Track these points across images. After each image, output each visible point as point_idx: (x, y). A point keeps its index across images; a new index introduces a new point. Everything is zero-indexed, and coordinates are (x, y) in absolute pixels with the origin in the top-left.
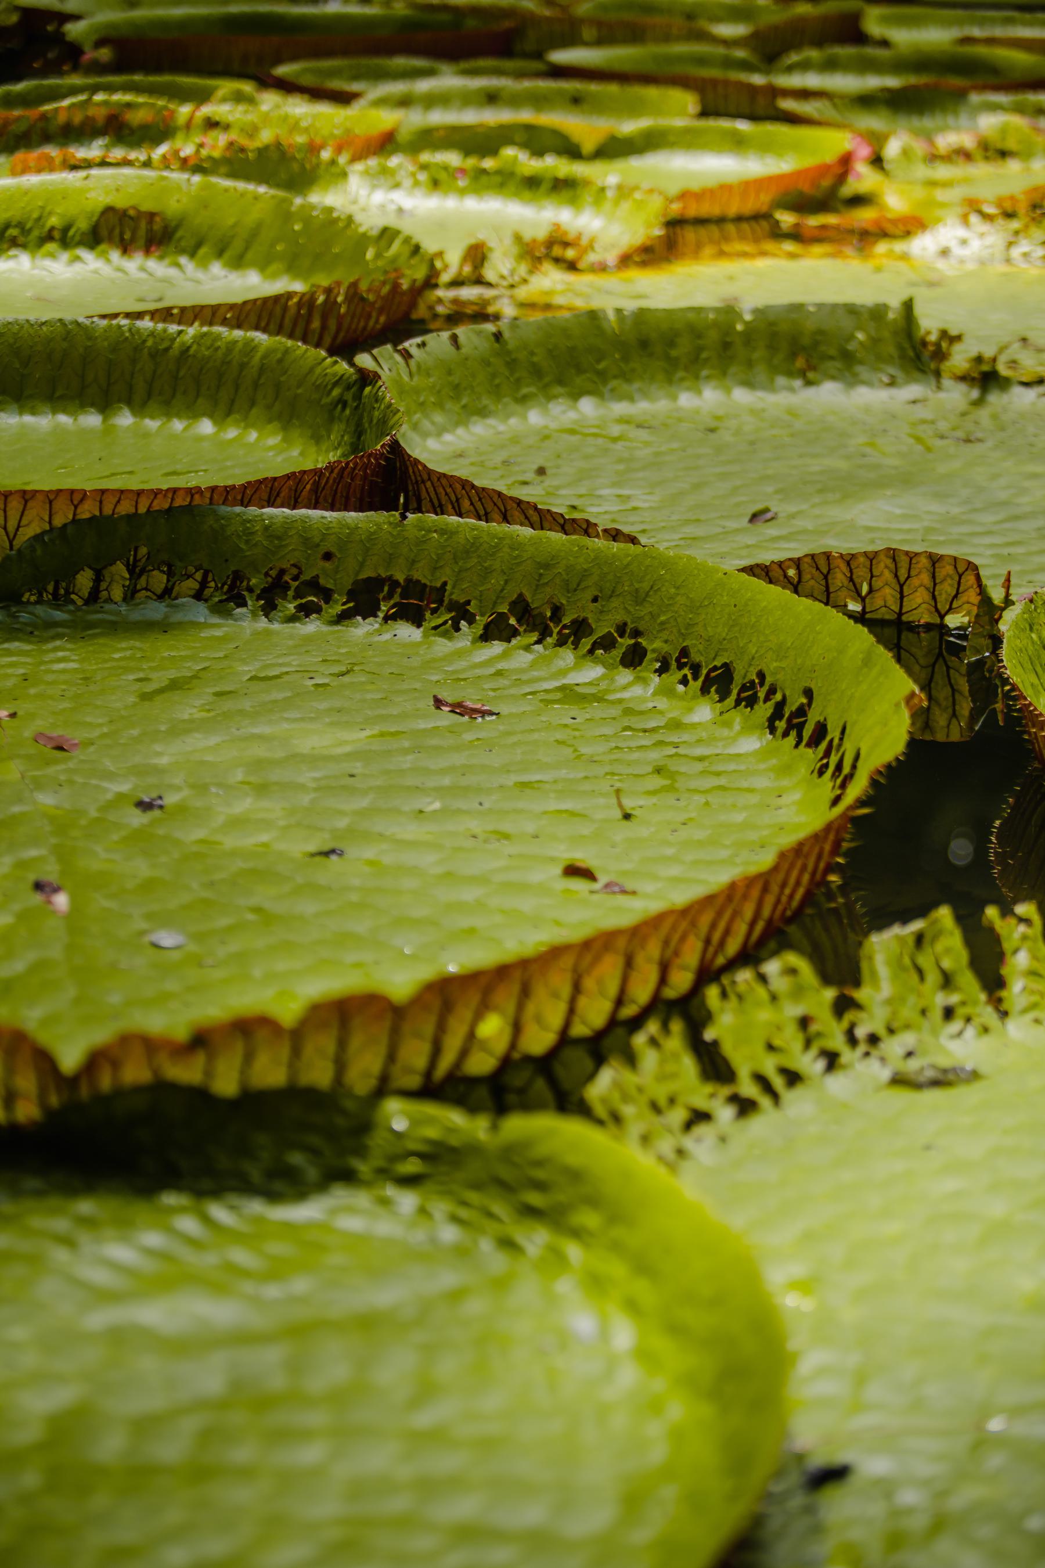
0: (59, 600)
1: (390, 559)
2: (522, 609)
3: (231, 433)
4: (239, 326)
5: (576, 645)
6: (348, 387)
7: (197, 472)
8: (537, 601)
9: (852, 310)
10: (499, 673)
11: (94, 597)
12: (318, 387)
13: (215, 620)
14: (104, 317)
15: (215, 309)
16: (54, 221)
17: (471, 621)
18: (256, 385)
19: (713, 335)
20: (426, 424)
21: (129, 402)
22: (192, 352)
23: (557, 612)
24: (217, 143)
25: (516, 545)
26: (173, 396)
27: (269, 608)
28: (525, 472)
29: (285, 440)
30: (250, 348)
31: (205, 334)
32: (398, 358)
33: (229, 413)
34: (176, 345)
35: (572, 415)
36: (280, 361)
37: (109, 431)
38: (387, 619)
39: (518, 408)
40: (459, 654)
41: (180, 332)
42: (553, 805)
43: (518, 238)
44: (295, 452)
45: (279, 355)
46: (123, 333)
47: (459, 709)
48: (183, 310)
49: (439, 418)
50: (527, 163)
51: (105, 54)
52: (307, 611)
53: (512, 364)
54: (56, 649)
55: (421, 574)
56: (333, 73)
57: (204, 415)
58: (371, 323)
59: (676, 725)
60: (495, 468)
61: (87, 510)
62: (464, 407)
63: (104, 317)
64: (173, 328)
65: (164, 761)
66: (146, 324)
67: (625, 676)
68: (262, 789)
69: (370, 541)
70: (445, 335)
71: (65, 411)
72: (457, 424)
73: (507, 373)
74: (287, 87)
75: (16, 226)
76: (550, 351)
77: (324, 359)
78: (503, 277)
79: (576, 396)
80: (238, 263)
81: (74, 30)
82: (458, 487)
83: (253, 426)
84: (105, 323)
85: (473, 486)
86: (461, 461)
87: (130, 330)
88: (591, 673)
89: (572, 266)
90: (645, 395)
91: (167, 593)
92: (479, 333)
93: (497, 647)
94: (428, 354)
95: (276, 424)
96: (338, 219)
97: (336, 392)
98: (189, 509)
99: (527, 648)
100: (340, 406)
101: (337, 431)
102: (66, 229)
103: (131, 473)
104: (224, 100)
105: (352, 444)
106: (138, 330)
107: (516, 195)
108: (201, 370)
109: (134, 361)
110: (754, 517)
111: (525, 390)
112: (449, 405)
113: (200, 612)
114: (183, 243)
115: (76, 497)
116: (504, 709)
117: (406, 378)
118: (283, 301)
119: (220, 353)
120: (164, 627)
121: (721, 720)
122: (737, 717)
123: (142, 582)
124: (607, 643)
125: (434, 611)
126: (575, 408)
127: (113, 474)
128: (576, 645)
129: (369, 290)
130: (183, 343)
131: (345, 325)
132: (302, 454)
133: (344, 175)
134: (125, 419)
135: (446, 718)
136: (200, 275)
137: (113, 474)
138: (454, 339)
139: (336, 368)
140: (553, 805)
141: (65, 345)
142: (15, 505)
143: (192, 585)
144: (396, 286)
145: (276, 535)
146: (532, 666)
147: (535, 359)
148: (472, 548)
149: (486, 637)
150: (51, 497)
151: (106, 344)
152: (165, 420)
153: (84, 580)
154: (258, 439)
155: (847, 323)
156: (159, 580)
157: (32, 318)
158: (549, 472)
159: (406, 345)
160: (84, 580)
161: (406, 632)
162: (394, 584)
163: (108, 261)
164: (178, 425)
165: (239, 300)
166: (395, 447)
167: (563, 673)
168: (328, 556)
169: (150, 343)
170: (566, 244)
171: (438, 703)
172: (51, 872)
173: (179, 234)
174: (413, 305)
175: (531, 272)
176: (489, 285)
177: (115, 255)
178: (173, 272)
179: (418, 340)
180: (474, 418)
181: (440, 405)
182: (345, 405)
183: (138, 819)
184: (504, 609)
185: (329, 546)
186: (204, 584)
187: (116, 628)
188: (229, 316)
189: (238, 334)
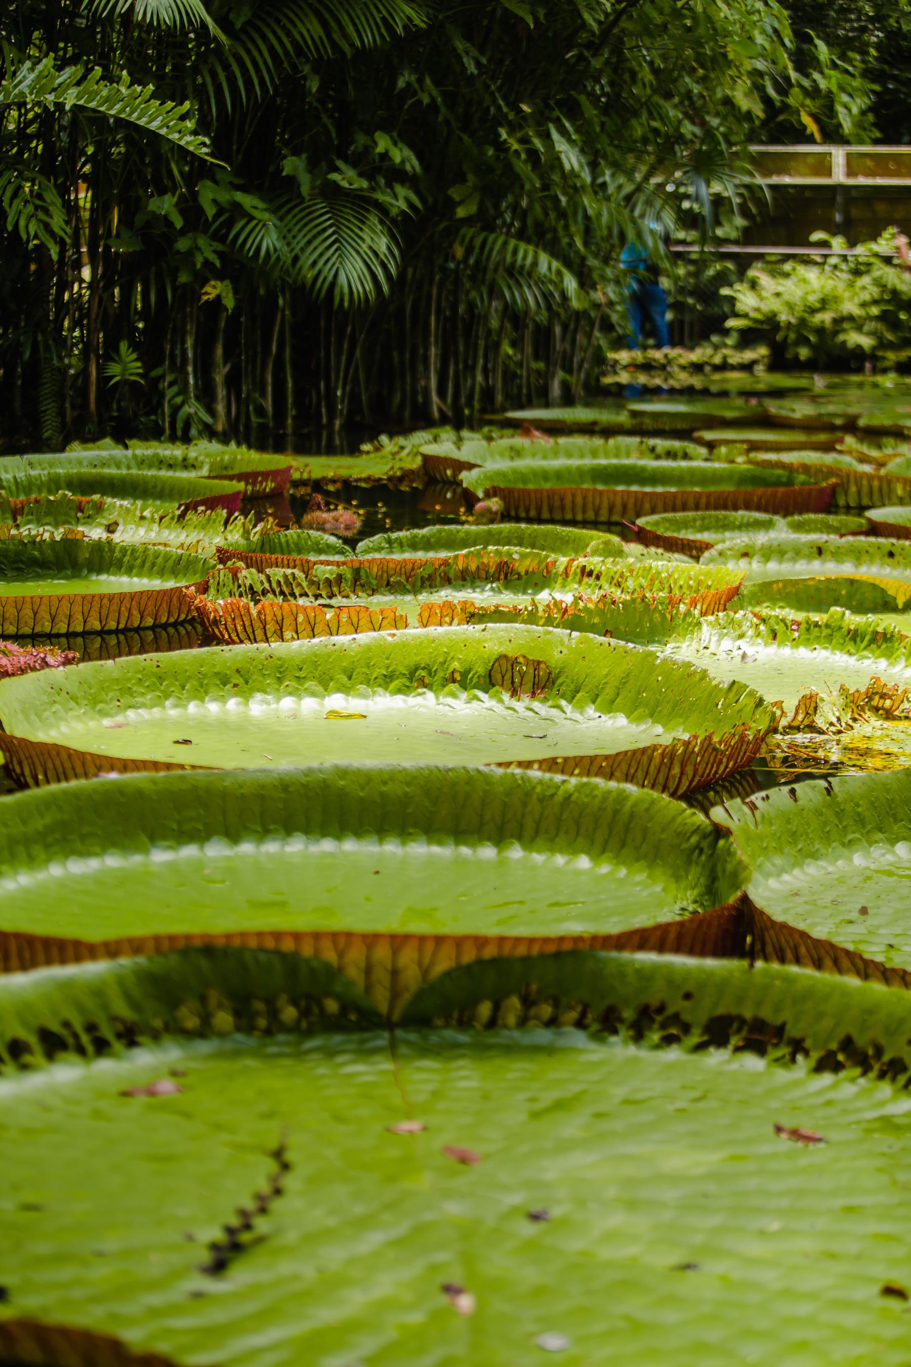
0: (465, 1023)
2: (847, 1044)
3: (605, 868)
4: (611, 776)
5: (893, 1080)
6: (704, 836)
7: (575, 903)
8: (862, 1041)
10: (829, 1103)
11: (492, 1023)
12: (678, 834)
13: (593, 1046)
14: (500, 765)
15: (593, 759)
16: (456, 665)
17: (807, 1053)
18: (627, 829)
20: (768, 866)
21: (520, 838)
22: (573, 798)
23: (879, 1051)
24: (591, 594)
25: (846, 993)
26: (557, 835)
27: (638, 1037)
28: (850, 911)
29: (650, 877)
30: (622, 797)
31: (585, 784)
32: (746, 809)
33: (603, 851)
34: (561, 792)
35: (889, 857)
36: (647, 810)
37: (502, 863)
38: (737, 1049)
39: (845, 851)
40: (796, 1084)
41: (564, 782)
42: (873, 1227)
43: (842, 688)
44: (658, 888)
45: (646, 805)
46: (516, 780)
47: (796, 1134)
48: (566, 759)
49: (778, 861)
50: (853, 620)
51: (495, 504)
52: (669, 1040)
53: (840, 814)
54: (462, 1068)
55: (766, 1014)
56: (685, 525)
57: (582, 851)
58: (722, 768)
60: (826, 907)
61: (489, 952)
62: (800, 850)
63: (500, 765)
64: (558, 778)
65: (549, 1176)
66: (535, 774)
68: (632, 1205)
69: (722, 985)
70: (786, 789)
71: (465, 843)
72: (794, 866)
73: (837, 822)
74: (645, 538)
75: (424, 668)
76: (872, 803)
77: (684, 810)
78: (832, 724)
79: (893, 841)
80: (609, 707)
81: (467, 478)
82: (797, 937)
83: (624, 863)
84: (500, 771)
85: (809, 937)
86: (797, 899)
87: (522, 778)
89: (889, 715)
91: (552, 1022)
92: (813, 788)
93: (827, 1078)
94: (771, 805)
95: (643, 863)
96: (695, 672)
97: (694, 839)
98: (574, 953)
99: (853, 1080)
100: (697, 852)
101: (695, 872)
102: (464, 674)
103: (521, 902)
104: (595, 552)
105: (707, 887)
106: (529, 780)
107: (841, 647)
108: (581, 813)
109: (525, 804)
111: (850, 837)
112: (787, 850)
113: (579, 1038)
114: (563, 688)
115: (480, 941)
116: (833, 1135)
117: (752, 827)
118: (650, 752)
119: (597, 801)
120: (549, 1050)
123: (533, 1012)
125: (776, 1046)
126: (893, 853)
127: (506, 904)
128: (893, 1080)
129: (720, 742)
130: (566, 791)
131: (700, 772)
132: (664, 890)
133: (699, 624)
134: (516, 852)
135: (784, 1143)
136: (577, 716)
137: (506, 904)
138: (793, 792)
139: (695, 818)
140: (873, 1227)
141: (467, 788)
142: (429, 947)
143: (574, 1015)
144: (742, 737)
145: (646, 976)
146: (858, 1096)
147: (860, 810)
149: (818, 1068)
150: (459, 942)
151: (501, 789)
152: (549, 854)
153: (485, 1009)
154: (627, 876)
156: (546, 1010)
157: (440, 764)
158: (870, 911)
159: (752, 798)
160: (485, 1009)
161: (752, 1062)
162: (742, 1021)
163: (501, 701)
164: (560, 860)
165: (613, 752)
166: (745, 900)
167: (882, 1104)
169: (538, 789)
170: (883, 696)
171: (779, 1129)
172: (456, 1276)
173: (559, 681)
174: (757, 749)
175: (855, 720)
177: (506, 696)
178: (555, 712)
179: (763, 794)
180: (808, 860)
181: (779, 850)
182: (701, 851)
183: (529, 1229)
184: (834, 1046)
185: (689, 987)
186: (583, 1015)
187: (510, 1050)
188: (604, 764)
189: (613, 784)
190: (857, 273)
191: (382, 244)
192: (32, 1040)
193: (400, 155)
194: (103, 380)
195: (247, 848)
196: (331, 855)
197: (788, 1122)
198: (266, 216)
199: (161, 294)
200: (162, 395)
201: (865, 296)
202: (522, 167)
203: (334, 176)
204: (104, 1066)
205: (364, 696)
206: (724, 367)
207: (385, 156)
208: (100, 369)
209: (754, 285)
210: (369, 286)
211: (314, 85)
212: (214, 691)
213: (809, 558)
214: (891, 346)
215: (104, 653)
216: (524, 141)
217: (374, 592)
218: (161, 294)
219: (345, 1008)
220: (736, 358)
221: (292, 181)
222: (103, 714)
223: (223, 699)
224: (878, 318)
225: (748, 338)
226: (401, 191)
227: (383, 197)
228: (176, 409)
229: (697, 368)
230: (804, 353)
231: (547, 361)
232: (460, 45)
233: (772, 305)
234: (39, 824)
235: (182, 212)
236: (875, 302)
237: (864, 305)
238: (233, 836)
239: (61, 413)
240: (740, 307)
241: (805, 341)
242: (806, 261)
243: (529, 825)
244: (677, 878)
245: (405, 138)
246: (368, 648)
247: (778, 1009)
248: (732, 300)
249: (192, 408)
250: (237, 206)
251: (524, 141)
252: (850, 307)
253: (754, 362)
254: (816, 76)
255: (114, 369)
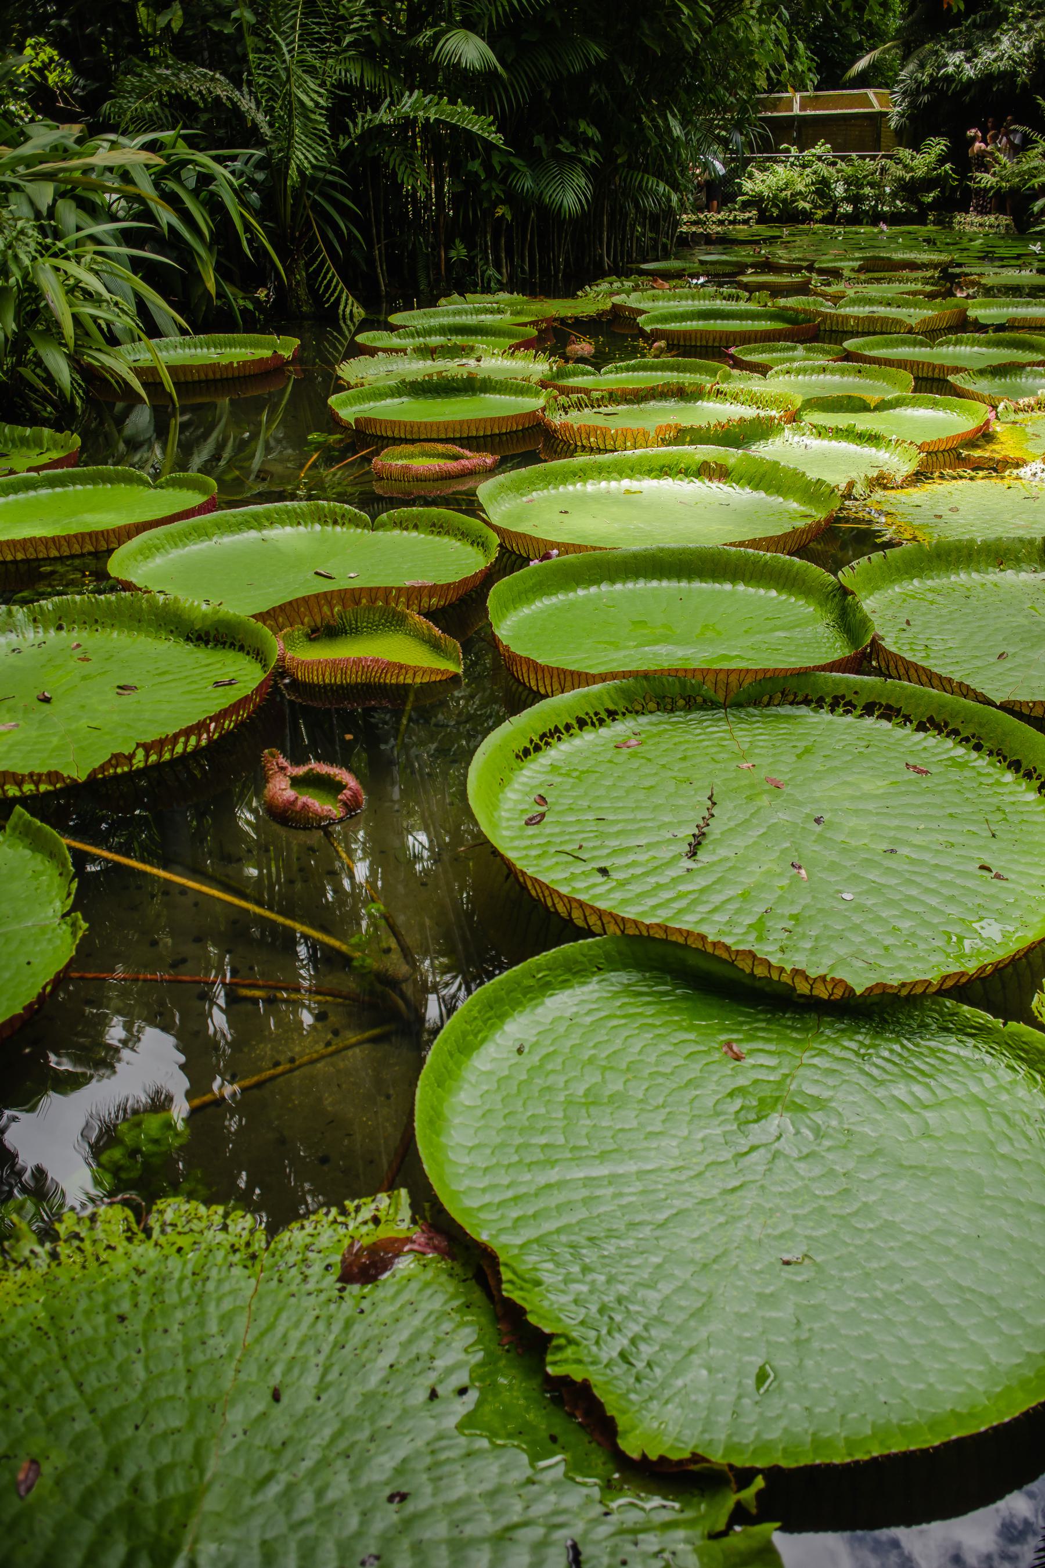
1: (880, 696)
2: (931, 719)
3: (784, 597)
9: (1021, 540)
10: (925, 749)
13: (812, 714)
17: (911, 722)
19: (965, 551)
23: (946, 725)
25: (930, 696)
52: (847, 712)
55: (892, 703)
59: (998, 783)
67: (974, 754)
74: (739, 364)
88: (960, 751)
89: (885, 487)
90: (938, 576)
93: (922, 735)
102: (686, 470)
110: (1000, 656)
116: (933, 769)
121: (1016, 782)
122: (1024, 783)
124: (967, 740)
135: (912, 775)
145: (837, 683)
148: (912, 695)
149: (917, 730)
153: (766, 699)
155: (1018, 546)
161: (885, 724)
162: (881, 705)
164: (762, 591)
168: (856, 693)
176: (856, 499)
190: (804, 166)
191: (583, 182)
192: (574, 723)
193: (592, 132)
194: (448, 259)
195: (619, 586)
196: (656, 589)
197: (911, 763)
198: (525, 169)
199: (475, 214)
200: (476, 265)
201: (808, 180)
202: (650, 133)
203: (559, 146)
204: (603, 731)
205: (638, 480)
206: (733, 222)
207: (584, 133)
208: (446, 254)
209: (751, 177)
210: (578, 207)
211: (548, 95)
212: (570, 480)
213: (819, 373)
214: (820, 207)
215: (518, 466)
216: (653, 120)
217: (619, 404)
218: (475, 214)
219: (705, 701)
220: (741, 216)
221: (539, 150)
222: (522, 495)
223: (574, 484)
224: (814, 192)
225: (745, 206)
226: (592, 152)
227: (584, 157)
228: (483, 272)
229: (721, 222)
230: (775, 212)
231: (657, 233)
232: (622, 68)
233: (760, 187)
234: (530, 583)
235: (485, 170)
236: (813, 184)
237: (807, 186)
238: (613, 581)
239: (428, 276)
240: (745, 189)
241: (777, 206)
242: (776, 161)
243: (748, 575)
244: (821, 606)
245: (594, 122)
246: (640, 457)
247: (897, 702)
248: (740, 185)
249: (491, 272)
250: (511, 164)
251: (653, 120)
252: (800, 187)
253: (750, 218)
254: (797, 63)
255: (453, 254)
